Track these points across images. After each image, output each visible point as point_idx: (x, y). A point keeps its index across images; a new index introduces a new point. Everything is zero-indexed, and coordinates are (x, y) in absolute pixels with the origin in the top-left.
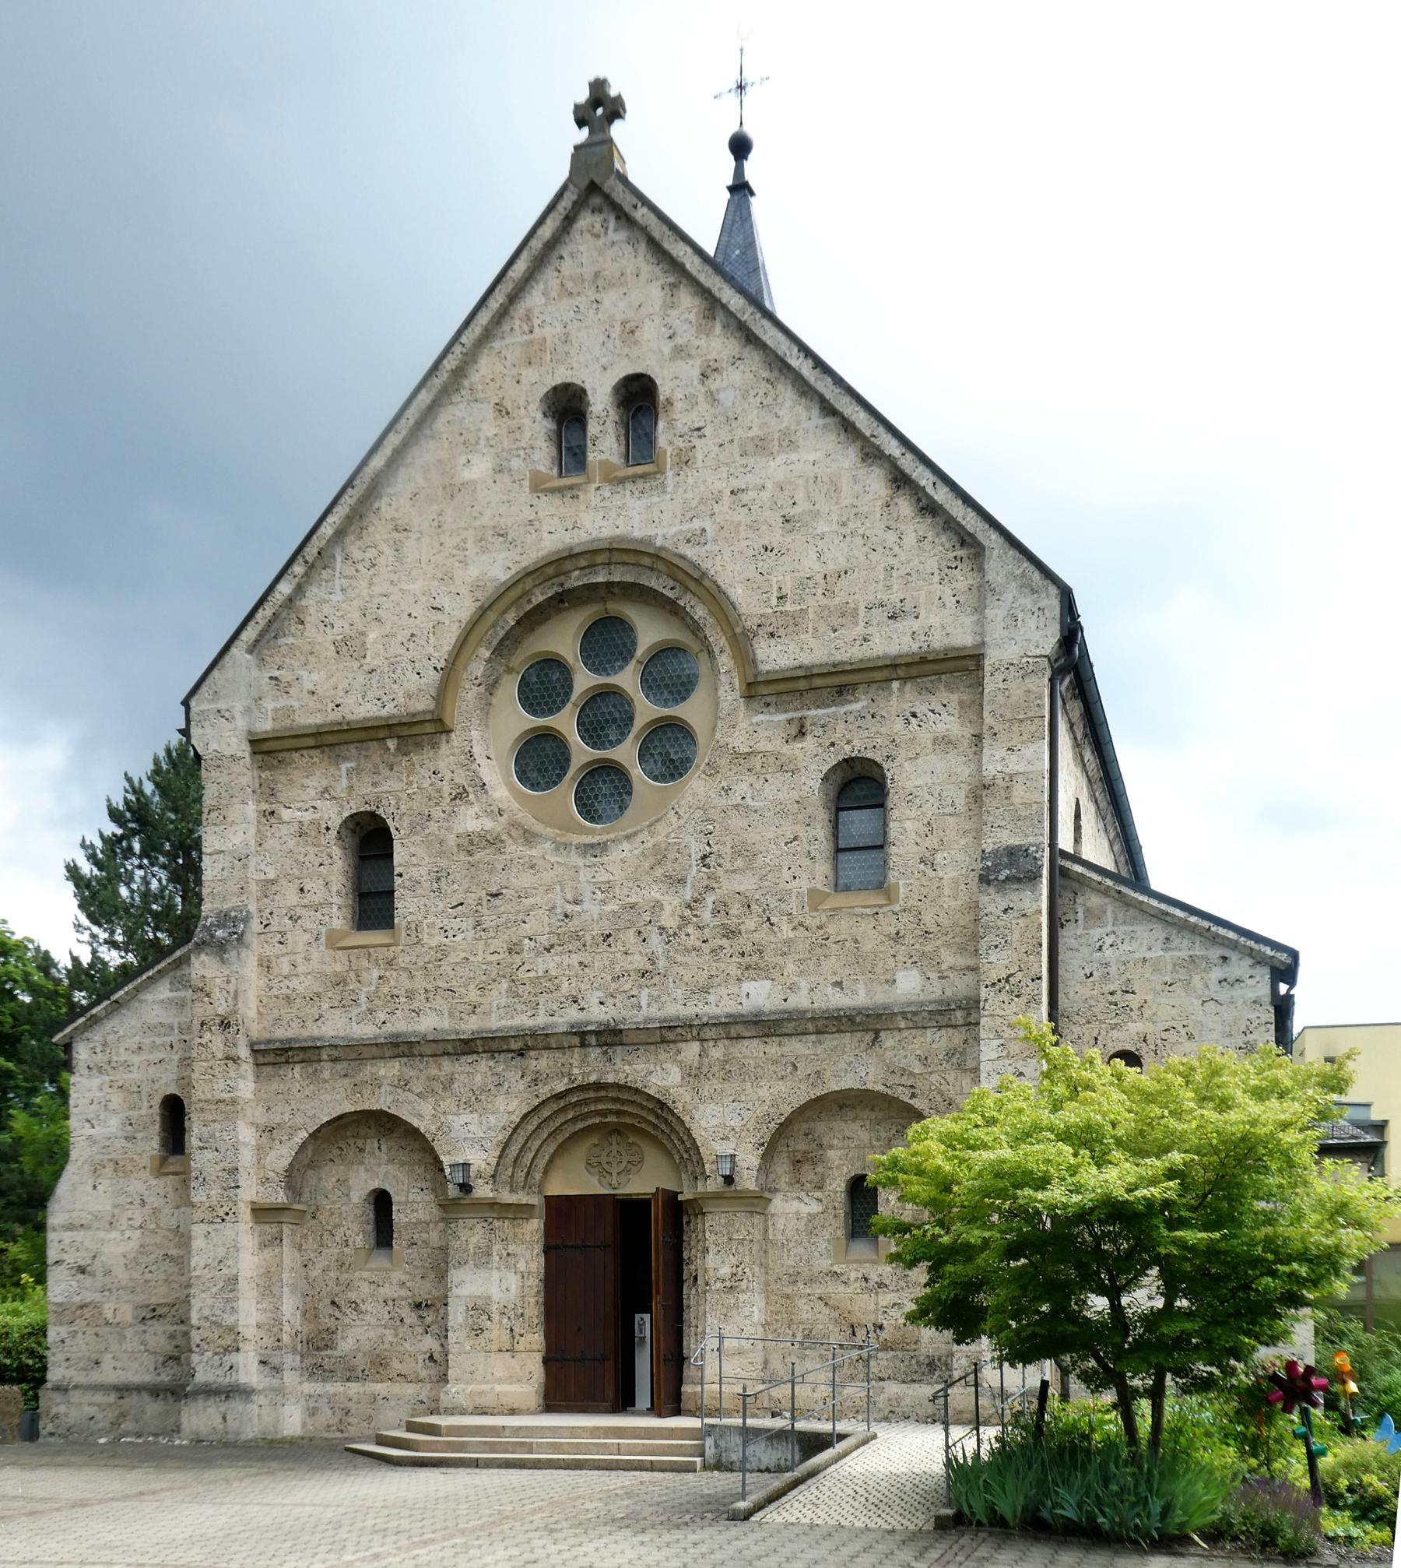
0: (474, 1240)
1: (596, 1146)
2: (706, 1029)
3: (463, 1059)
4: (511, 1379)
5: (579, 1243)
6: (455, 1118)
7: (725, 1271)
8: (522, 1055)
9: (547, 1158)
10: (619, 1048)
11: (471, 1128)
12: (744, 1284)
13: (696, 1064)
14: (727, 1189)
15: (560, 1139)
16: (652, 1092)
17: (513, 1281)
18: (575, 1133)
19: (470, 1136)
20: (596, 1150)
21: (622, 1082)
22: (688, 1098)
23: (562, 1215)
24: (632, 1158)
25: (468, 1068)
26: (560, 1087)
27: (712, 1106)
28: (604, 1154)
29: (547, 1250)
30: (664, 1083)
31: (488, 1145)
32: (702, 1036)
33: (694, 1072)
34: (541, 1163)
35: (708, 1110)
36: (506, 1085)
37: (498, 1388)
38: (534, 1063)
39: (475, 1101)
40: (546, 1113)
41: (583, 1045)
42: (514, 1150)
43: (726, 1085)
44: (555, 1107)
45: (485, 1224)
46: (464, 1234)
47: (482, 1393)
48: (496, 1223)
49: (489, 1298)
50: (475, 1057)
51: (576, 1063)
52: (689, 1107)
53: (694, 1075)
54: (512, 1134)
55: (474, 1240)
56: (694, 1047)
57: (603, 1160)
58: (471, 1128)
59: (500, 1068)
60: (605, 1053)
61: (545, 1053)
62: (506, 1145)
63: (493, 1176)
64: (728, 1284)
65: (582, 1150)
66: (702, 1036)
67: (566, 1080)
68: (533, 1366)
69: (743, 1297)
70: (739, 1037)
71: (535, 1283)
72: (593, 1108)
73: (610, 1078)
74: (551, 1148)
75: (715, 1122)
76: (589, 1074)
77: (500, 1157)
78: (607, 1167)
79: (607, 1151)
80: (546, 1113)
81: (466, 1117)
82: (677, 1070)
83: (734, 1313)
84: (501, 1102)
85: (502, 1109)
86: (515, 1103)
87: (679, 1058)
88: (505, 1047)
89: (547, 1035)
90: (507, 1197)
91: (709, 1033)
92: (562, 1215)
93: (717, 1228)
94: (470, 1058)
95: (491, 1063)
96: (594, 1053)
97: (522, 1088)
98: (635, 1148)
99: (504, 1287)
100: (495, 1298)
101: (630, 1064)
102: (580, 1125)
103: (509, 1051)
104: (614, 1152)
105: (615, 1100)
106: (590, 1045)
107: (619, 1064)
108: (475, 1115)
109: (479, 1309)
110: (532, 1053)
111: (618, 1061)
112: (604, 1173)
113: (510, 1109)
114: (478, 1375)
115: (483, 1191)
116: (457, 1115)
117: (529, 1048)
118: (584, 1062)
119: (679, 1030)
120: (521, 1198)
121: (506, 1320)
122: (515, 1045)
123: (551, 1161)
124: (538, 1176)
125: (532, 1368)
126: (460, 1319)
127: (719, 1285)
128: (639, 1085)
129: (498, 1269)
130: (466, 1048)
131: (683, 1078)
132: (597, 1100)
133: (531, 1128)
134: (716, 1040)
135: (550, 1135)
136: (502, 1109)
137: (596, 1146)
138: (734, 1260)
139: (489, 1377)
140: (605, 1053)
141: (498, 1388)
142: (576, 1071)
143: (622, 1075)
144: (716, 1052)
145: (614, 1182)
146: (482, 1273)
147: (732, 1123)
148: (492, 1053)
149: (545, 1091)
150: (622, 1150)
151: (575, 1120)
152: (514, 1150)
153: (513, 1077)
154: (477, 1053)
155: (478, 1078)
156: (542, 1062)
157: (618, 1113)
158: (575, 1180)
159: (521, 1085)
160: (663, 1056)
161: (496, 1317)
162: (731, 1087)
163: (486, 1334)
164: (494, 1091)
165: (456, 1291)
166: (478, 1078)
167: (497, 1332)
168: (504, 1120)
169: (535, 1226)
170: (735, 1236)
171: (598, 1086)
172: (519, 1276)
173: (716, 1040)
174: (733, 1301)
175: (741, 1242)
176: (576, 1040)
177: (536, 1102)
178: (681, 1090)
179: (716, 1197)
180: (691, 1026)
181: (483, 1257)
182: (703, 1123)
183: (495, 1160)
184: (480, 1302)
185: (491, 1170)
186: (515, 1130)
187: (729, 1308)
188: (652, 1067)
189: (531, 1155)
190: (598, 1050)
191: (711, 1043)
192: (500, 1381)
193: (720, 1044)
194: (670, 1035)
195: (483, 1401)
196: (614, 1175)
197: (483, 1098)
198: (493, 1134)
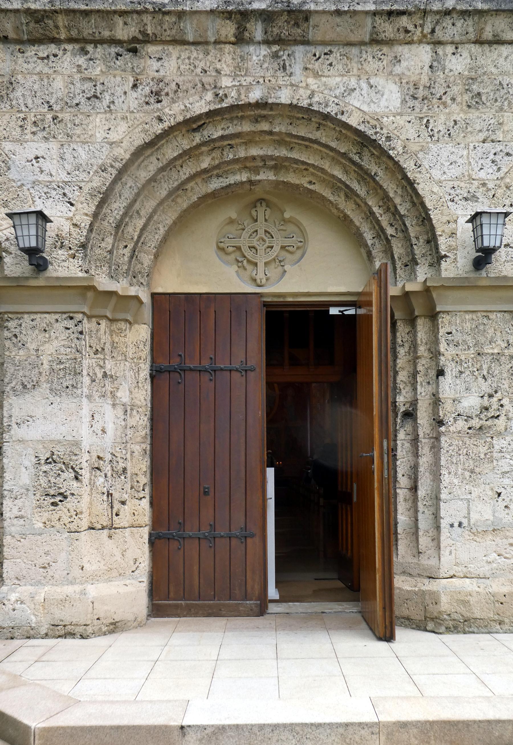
0: (49, 349)
1: (231, 222)
2: (447, 22)
3: (31, 51)
4: (113, 573)
5: (206, 363)
6: (17, 148)
7: (471, 402)
8: (134, 51)
9: (162, 231)
10: (299, 50)
11: (46, 165)
12: (501, 422)
13: (425, 80)
14: (472, 275)
15: (184, 203)
16: (353, 121)
17: (110, 418)
18: (214, 194)
19: (43, 177)
20: (233, 230)
21: (304, 103)
22: (410, 132)
23: (177, 320)
24: (287, 242)
25: (40, 66)
26: (200, 105)
27: (450, 147)
28: (245, 234)
29: (155, 375)
30: (373, 108)
31: (74, 195)
32: (439, 34)
33: (421, 93)
34: (153, 240)
35: (444, 154)
36: (107, 98)
37: (93, 591)
38: (155, 65)
39: (50, 122)
40: (170, 151)
41: (241, 39)
42: (117, 207)
43: (473, 114)
44: (186, 144)
45: (70, 324)
46: (32, 339)
47: (65, 600)
48: (86, 325)
49: (77, 444)
50: (53, 48)
51: (226, 70)
52: (413, 147)
53: (419, 96)
54: (114, 182)
55: (49, 349)
56: (423, 54)
57: (244, 242)
58: (46, 165)
59: (96, 70)
60: (275, 56)
61: (174, 51)
62: (104, 199)
63: (83, 246)
64: (476, 423)
65: (211, 227)
66: (439, 34)
67: (209, 96)
68: (136, 548)
69: (499, 443)
70: (497, 41)
71: (141, 420)
72: (242, 153)
73: (284, 97)
74: (169, 217)
75: (454, 172)
76: (249, 88)
77: (95, 215)
78: (249, 254)
79: (249, 229)
80: (170, 151)
81: (36, 147)
82: (394, 88)
83: (486, 467)
84: (98, 125)
85: (99, 136)
86: (123, 127)
87: (398, 69)
88: (106, 34)
89: (181, 15)
90: (103, 282)
91: (451, 30)
92: (177, 320)
93: (458, 337)
94: (44, 50)
95: (81, 60)
96: (258, 54)
97: (133, 104)
98: (291, 228)
99: (97, 427)
100: (85, 445)
101: (317, 75)
102: (215, 184)
103: (113, 42)
104: (261, 233)
105: (281, 140)
106: (250, 41)
107: (298, 75)
108: (54, 145)
109: (57, 461)
110: (152, 49)
111: (297, 69)
112: (243, 260)
113: (114, 136)
114: (58, 570)
115: (65, 267)
116: (20, 141)
117: (146, 39)
118: (239, 70)
119: (404, 21)
120: (121, 286)
121: (102, 480)
122: (123, 31)
123: (165, 240)
124: (147, 259)
125: (138, 553)
126: (25, 478)
127: (461, 424)
128: (332, 110)
129: (89, 397)
130: (37, 30)
131: (404, 101)
132: (249, 139)
133: (144, 175)
134: (456, 45)
135: (170, 194)
136: (99, 136)
137: (231, 222)
138: (485, 387)
139: (76, 572)
140: (275, 56)
141: (93, 591)
142: (226, 82)
143: (304, 93)
144: (458, 64)
145: (260, 276)
146: (67, 403)
147: (482, 174)
148: (82, 42)
149: (174, 112)
150: (273, 230)
151: (205, 174)
152: (117, 207)
153: (118, 83)
154: (54, 40)
155: (59, 83)
156: (168, 64)
157: (279, 165)
158: (201, 271)
159: (134, 99)
160: (372, 65)
161: (86, 474)
162: (481, 118)
163: (70, 503)
164: (85, 107)
165: (17, 433)
166: (59, 83)
167: (86, 500)
168: (103, 156)
169: (142, 333)
170: (487, 350)
171: (263, 108)
172: (120, 411)
173: (456, 45)
174: (483, 450)
175: (496, 358)
176: (229, 30)
177: (158, 128)
178: (401, 121)
179: (460, 285)
180: (425, 13)
181: (65, 378)
182: (436, 174)
183: (88, 221)
184: (60, 451)
185: (79, 236)
186: (121, 172)
187: (478, 460)
188: (353, 82)
189: (140, 223)
190: (264, 50)
191: (450, 49)
192: (94, 578)
193: (465, 51)
194: (387, 29)
195: (65, 615)
196: (261, 266)
197: (66, 116)
198: (83, 176)
